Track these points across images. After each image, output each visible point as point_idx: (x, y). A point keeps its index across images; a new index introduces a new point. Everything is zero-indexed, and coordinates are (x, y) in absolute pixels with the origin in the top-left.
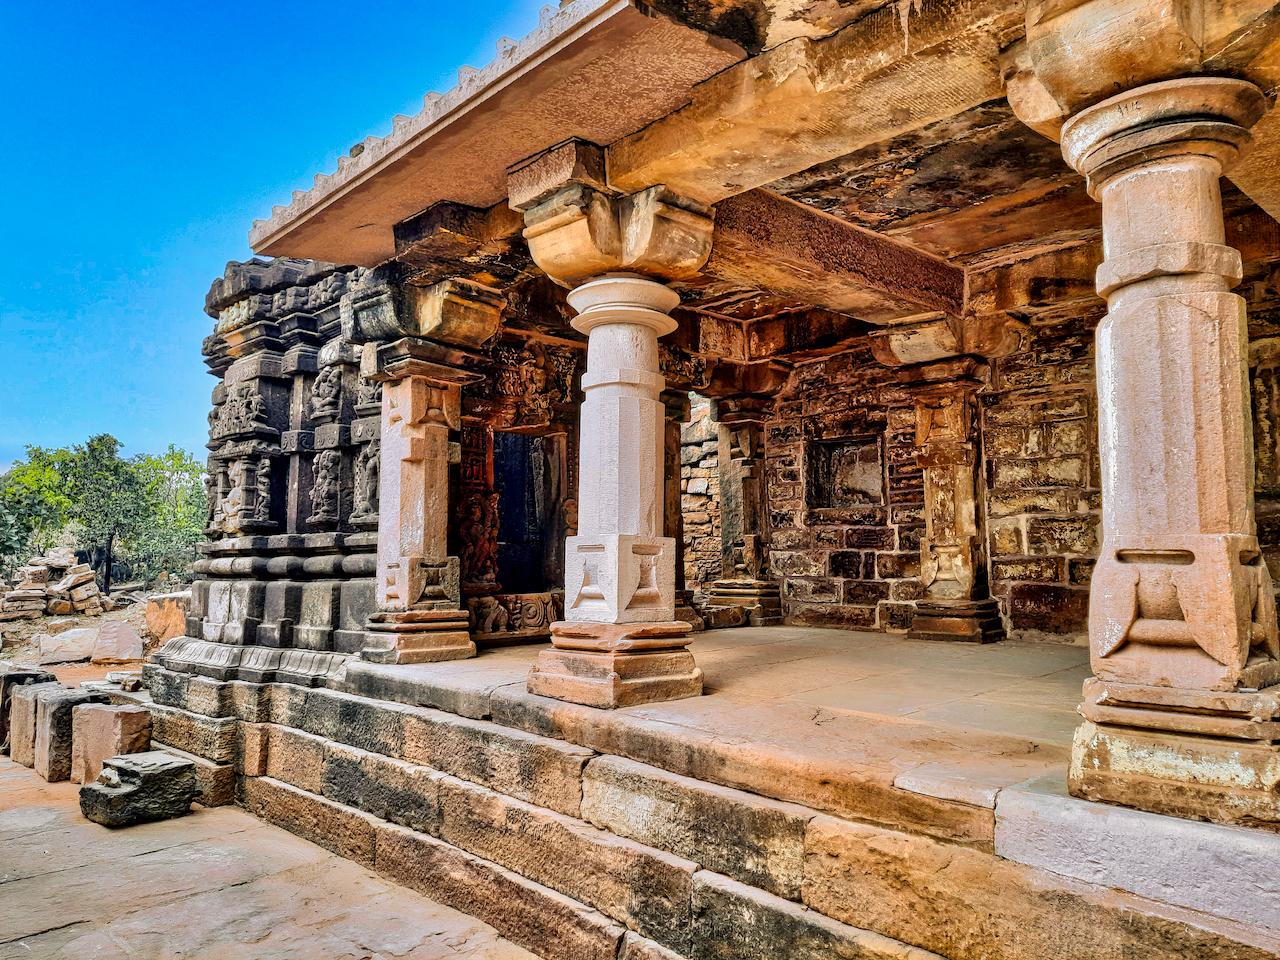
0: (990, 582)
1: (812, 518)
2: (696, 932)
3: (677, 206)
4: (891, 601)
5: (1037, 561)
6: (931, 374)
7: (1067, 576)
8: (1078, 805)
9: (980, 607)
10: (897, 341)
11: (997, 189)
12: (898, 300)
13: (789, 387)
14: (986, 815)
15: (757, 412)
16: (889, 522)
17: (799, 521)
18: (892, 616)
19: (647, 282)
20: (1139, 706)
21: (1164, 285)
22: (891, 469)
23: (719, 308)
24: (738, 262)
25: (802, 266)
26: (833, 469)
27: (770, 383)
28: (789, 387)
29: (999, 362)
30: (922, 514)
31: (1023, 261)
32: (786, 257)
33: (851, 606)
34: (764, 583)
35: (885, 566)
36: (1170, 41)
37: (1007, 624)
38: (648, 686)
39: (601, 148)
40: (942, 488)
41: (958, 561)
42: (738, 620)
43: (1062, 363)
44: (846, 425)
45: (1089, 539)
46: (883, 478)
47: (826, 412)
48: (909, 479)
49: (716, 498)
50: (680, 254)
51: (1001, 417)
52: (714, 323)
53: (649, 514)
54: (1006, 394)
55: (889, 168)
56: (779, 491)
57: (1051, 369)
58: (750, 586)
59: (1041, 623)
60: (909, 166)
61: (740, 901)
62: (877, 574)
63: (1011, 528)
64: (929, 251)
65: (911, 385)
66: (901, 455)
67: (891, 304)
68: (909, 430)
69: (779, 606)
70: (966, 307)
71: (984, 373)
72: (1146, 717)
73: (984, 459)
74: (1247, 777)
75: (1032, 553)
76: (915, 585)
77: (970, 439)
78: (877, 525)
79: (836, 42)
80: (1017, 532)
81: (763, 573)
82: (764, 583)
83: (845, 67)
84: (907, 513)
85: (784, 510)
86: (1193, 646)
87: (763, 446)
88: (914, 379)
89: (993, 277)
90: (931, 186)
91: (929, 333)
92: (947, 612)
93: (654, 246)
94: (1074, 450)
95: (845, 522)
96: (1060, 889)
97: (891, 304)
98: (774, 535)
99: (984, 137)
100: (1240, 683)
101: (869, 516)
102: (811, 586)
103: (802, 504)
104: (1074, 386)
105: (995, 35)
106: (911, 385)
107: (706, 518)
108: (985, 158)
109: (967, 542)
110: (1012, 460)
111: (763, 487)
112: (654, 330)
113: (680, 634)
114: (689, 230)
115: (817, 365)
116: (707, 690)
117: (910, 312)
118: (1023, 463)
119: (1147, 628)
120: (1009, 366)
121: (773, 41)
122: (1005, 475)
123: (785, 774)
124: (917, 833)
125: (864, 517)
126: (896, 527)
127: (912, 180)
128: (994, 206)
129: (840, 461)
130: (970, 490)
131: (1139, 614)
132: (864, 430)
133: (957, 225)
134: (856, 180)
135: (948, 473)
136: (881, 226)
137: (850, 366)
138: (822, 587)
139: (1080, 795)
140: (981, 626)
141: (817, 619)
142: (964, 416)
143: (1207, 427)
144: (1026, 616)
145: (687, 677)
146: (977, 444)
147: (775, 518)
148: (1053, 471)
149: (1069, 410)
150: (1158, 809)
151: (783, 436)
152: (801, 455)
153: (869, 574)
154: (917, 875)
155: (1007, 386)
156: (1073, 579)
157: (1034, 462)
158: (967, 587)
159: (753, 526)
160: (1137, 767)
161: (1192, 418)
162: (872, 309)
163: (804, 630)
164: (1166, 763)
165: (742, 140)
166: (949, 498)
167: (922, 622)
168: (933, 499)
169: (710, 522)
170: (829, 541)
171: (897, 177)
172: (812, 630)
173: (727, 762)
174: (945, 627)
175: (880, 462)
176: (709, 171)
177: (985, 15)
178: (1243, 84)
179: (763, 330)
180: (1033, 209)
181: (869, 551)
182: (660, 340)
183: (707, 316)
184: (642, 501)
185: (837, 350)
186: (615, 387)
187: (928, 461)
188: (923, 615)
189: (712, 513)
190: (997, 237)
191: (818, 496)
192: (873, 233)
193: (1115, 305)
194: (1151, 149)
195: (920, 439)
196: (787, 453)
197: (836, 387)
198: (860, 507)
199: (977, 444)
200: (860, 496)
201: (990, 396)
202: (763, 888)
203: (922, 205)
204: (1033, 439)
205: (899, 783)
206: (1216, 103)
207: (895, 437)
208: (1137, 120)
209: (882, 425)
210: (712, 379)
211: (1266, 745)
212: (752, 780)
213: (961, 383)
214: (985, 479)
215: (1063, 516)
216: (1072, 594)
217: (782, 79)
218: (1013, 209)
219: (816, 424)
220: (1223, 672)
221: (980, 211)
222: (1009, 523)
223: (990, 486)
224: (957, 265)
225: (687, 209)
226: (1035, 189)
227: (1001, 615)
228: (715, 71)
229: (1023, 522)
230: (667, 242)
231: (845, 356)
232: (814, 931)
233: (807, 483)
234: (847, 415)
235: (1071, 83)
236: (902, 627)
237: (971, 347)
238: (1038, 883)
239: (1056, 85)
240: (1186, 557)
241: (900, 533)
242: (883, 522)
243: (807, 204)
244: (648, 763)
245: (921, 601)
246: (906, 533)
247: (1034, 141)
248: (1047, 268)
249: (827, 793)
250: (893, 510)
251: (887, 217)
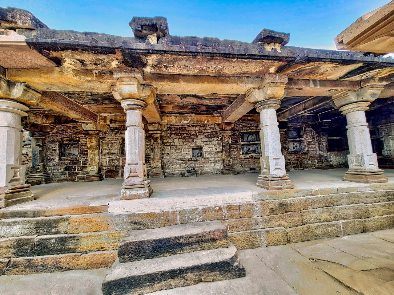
0: (101, 170)
1: (60, 159)
2: (36, 250)
3: (30, 88)
4: (80, 175)
5: (110, 166)
6: (91, 133)
7: (115, 168)
8: (122, 201)
9: (99, 175)
10: (83, 126)
11: (106, 104)
12: (85, 118)
13: (54, 131)
14: (107, 206)
15: (45, 136)
16: (80, 160)
17: (56, 160)
18: (80, 178)
19: (17, 103)
20: (131, 185)
21: (135, 127)
22: (81, 150)
23: (33, 111)
24: (46, 103)
25: (63, 108)
26: (66, 149)
27: (49, 129)
28: (54, 131)
29: (104, 132)
30: (87, 158)
31: (109, 116)
32: (59, 105)
33: (70, 177)
34: (46, 174)
35: (79, 169)
36: (137, 95)
37: (104, 177)
38: (17, 200)
39: (5, 69)
40: (92, 154)
41: (95, 167)
42: (38, 183)
43: (115, 134)
44: (70, 140)
45: (119, 162)
46: (79, 152)
47: (65, 137)
48: (85, 152)
49: (30, 155)
50: (31, 99)
51: (104, 142)
52: (32, 114)
53: (17, 159)
54: (105, 138)
55: (86, 95)
56: (51, 154)
57: (113, 134)
58: (42, 175)
59: (110, 176)
60: (90, 96)
61: (51, 238)
62: (77, 170)
63: (105, 161)
64: (91, 111)
65: (85, 134)
66: (83, 147)
67: (83, 119)
68: (85, 142)
69: (50, 179)
70: (98, 122)
71: (101, 133)
72: (131, 187)
73: (101, 149)
74: (144, 192)
75: (109, 165)
76: (85, 172)
77: (98, 145)
78: (77, 160)
79: (79, 72)
80: (106, 161)
81: (45, 172)
82: (46, 174)
83: (81, 77)
84: (84, 158)
85: (52, 158)
86: (138, 176)
87: (46, 143)
88: (87, 133)
89: (103, 117)
90: (94, 100)
91: (91, 125)
92: (92, 176)
93: (23, 95)
94: (117, 148)
95: (69, 160)
96: (119, 214)
97: (83, 119)
98: (49, 163)
99: (105, 95)
100: (143, 180)
101: (75, 159)
102: (59, 174)
103: (57, 156)
104: (117, 138)
105: (111, 83)
106: (85, 134)
107: (26, 159)
108: (105, 99)
109: (97, 163)
110: (106, 149)
111: (46, 153)
112: (21, 115)
113: (27, 187)
114: (34, 94)
115: (63, 127)
116: (35, 199)
117: (86, 121)
118: (108, 150)
119: (132, 174)
120: (106, 133)
121: (64, 66)
122: (104, 152)
123: (63, 210)
124: (94, 213)
125: (74, 159)
126: (81, 161)
127: (91, 98)
128: (105, 106)
129: (68, 148)
130: (98, 154)
131: (131, 173)
132: (74, 142)
133: (98, 108)
134: (78, 95)
135: (93, 151)
136: (82, 104)
137: (71, 129)
138: (62, 174)
139: (122, 200)
140: (99, 178)
141: (61, 181)
142: (97, 141)
143: (140, 147)
144: (107, 175)
145: (30, 197)
146: (99, 146)
147: (49, 160)
148: (113, 151)
149: (116, 141)
150: (133, 199)
151: (52, 141)
152: (57, 146)
153: (75, 170)
154: (93, 220)
155: (105, 136)
156: (116, 169)
157: (110, 150)
158: (97, 171)
159: (43, 161)
160: (130, 194)
161: (138, 146)
162: (78, 119)
163: (58, 183)
164: (134, 192)
165: (52, 81)
166: (93, 156)
167: (87, 178)
168: (90, 156)
169: (27, 161)
170: (65, 164)
171: (87, 97)
172: (59, 183)
173: (47, 212)
174: (92, 179)
175: (78, 148)
176: (43, 84)
177: (109, 80)
178: (145, 103)
179: (48, 118)
180: (112, 108)
181: (75, 166)
182: (21, 117)
183: (30, 112)
184: (15, 156)
185: (67, 125)
186: (6, 127)
187: (89, 149)
188: (87, 177)
189: (28, 159)
190: (105, 111)
191: (62, 154)
192: (80, 105)
193: (128, 129)
194: (134, 108)
195: (88, 144)
196: (53, 145)
197: (68, 132)
198: (72, 157)
199: (99, 146)
200: (73, 155)
201: (102, 138)
202: (57, 234)
203: (91, 103)
204: (110, 146)
205: (90, 205)
206: (142, 105)
207: (82, 144)
208: (132, 104)
209: (79, 141)
210: (31, 127)
211: (146, 188)
212: (54, 214)
213: (97, 135)
214: (101, 152)
215: (114, 159)
216: (116, 171)
217: (66, 74)
218: (108, 108)
219: (62, 140)
220: (141, 179)
221: (102, 106)
222: (105, 160)
223: (102, 153)
224: (97, 114)
225: (34, 90)
226: (112, 105)
227: (103, 176)
228: (47, 65)
229: (108, 160)
230: (27, 96)
231: (70, 126)
232: (70, 237)
233: (59, 152)
234: (70, 138)
235: (123, 95)
236: (82, 180)
237: (99, 129)
238: (115, 214)
239: (121, 95)
240: (137, 164)
241: (82, 162)
242: (78, 160)
243: (65, 96)
244: (19, 218)
245: (87, 175)
246: (84, 162)
247: (113, 99)
248: (113, 118)
249: (74, 211)
250: (81, 157)
251: (84, 103)
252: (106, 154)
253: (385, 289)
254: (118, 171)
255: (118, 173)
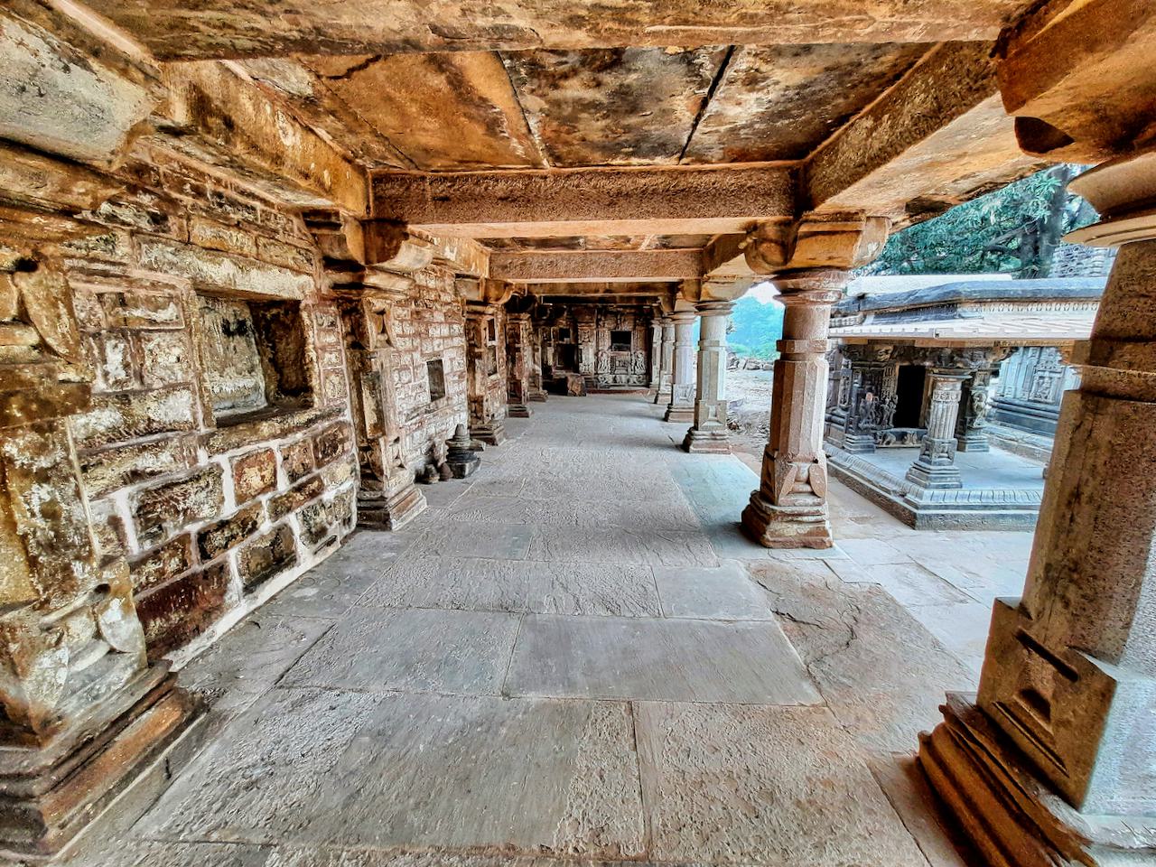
80: (115, 523)
204: (115, 357)
215: (182, 476)
229: (124, 502)
241: (239, 474)
252: (93, 453)
253: (1151, 862)
254: (222, 569)
255: (220, 579)
